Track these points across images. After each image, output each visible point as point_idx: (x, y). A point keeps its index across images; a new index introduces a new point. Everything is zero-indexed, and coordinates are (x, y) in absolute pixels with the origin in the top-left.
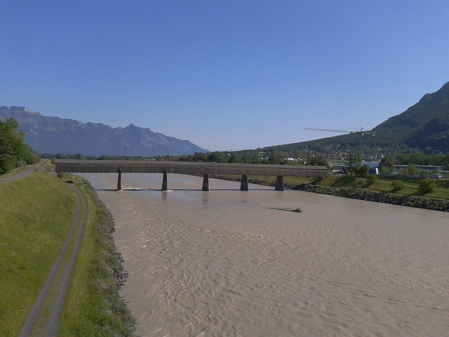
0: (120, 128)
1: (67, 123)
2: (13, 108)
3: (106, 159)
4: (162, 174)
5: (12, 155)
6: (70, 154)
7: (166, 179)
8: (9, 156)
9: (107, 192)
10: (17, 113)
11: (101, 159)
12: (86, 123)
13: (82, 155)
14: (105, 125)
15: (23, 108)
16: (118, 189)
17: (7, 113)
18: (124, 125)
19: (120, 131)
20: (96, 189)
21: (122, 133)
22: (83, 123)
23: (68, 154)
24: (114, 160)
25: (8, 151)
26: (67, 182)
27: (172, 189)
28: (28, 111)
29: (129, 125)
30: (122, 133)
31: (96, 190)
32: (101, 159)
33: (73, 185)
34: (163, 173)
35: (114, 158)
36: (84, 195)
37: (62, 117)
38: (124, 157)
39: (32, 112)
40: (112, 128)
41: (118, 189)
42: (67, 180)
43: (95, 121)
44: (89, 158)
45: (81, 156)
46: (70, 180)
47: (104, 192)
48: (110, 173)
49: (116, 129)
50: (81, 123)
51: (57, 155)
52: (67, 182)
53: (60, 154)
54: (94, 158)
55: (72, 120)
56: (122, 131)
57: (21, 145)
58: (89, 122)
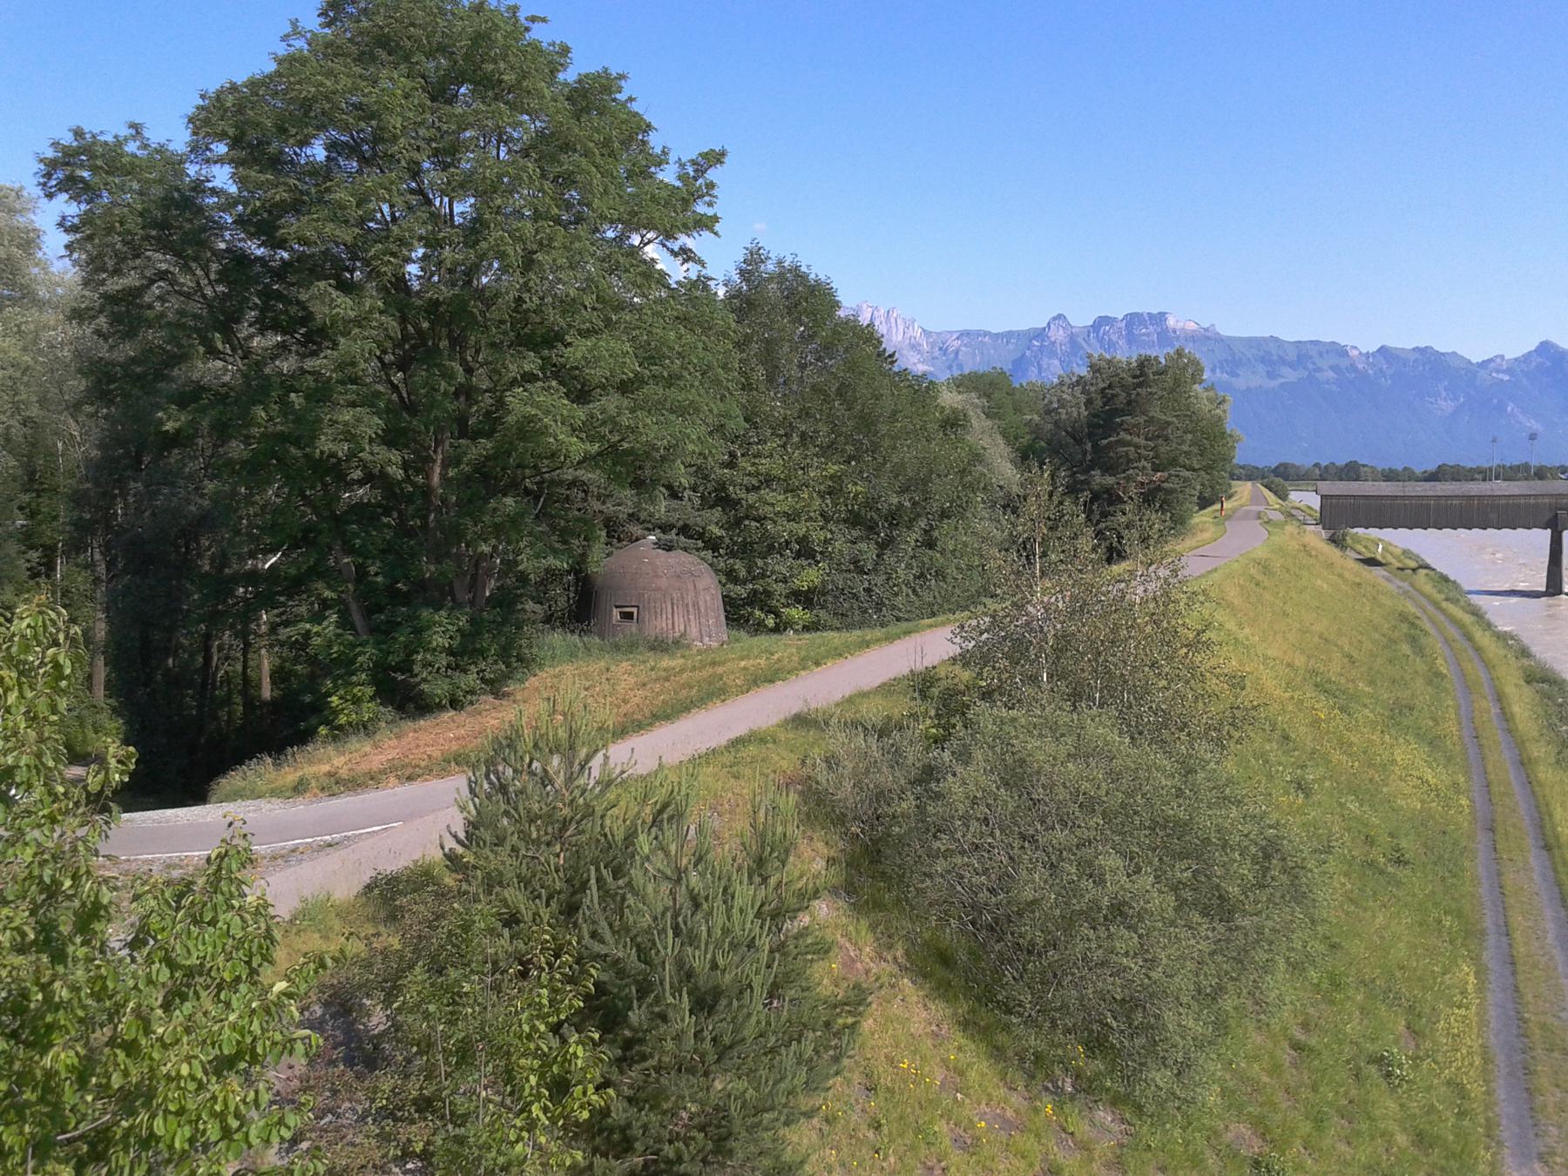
0: (1499, 360)
1: (1305, 354)
2: (1133, 319)
3: (1454, 479)
4: (1545, 535)
5: (1194, 470)
6: (1324, 464)
7: (1561, 553)
8: (1187, 474)
9: (1514, 600)
10: (1144, 334)
11: (1433, 477)
12: (1373, 348)
13: (1364, 466)
14: (1443, 354)
15: (1162, 316)
16: (1551, 590)
17: (1114, 338)
18: (1516, 344)
19: (1498, 371)
20: (1466, 588)
21: (1506, 378)
22: (1364, 351)
23: (1316, 465)
24: (1484, 480)
25: (1181, 459)
26: (1361, 560)
27: (1506, 587)
28: (1181, 325)
29: (1537, 344)
30: (1506, 378)
31: (1471, 592)
32: (1433, 477)
33: (1386, 573)
34: (1549, 531)
35: (1485, 474)
36: (1443, 611)
37: (1289, 335)
38: (1526, 467)
39: (1191, 326)
40: (1469, 361)
41: (1551, 590)
42: (1359, 553)
43: (1404, 339)
44: (1390, 476)
45: (1362, 469)
46: (1369, 555)
47: (1497, 601)
48: (1519, 530)
49: (1484, 364)
50: (1355, 353)
51: (1277, 468)
52: (1361, 560)
53: (1285, 466)
54: (1408, 476)
55: (1324, 344)
56: (1507, 371)
57: (1223, 438)
58: (1382, 347)
